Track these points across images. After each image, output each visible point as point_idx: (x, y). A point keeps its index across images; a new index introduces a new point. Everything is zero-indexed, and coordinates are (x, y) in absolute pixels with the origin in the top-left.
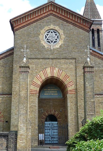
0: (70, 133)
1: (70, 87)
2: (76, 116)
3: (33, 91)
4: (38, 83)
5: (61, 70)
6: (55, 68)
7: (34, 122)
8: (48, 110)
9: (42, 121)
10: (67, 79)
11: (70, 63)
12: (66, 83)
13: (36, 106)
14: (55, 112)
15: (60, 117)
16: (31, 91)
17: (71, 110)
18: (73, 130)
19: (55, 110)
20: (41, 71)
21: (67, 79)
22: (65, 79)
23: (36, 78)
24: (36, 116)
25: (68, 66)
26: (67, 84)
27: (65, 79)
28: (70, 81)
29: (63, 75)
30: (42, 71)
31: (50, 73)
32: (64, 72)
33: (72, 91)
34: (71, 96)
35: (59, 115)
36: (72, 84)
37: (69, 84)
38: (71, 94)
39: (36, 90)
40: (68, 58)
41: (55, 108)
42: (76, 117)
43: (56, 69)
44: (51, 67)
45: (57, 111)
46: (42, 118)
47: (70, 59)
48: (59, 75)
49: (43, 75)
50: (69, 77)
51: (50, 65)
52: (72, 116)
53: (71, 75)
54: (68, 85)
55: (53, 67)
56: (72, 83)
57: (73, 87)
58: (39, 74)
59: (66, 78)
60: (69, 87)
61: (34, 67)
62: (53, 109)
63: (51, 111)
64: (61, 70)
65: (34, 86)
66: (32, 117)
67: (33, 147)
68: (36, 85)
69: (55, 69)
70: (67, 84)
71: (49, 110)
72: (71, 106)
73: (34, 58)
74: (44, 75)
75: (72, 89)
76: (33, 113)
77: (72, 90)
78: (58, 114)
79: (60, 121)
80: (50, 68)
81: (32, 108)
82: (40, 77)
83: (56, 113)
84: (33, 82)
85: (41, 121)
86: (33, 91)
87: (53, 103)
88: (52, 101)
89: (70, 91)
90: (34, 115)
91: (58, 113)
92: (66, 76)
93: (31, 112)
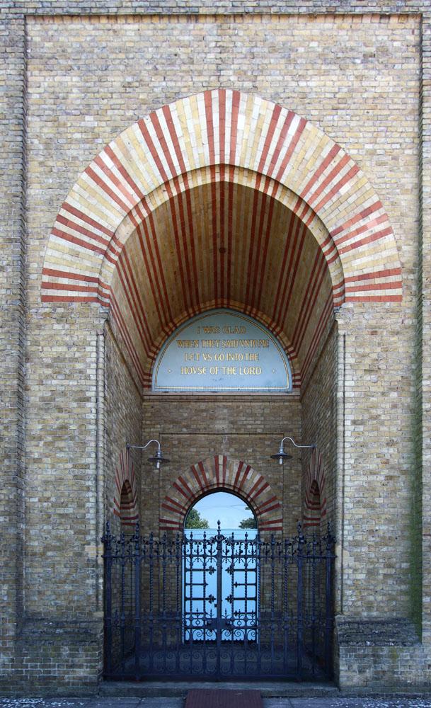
0: (348, 592)
1: (362, 254)
2: (404, 472)
3: (65, 281)
4: (103, 216)
5: (291, 115)
6: (243, 96)
7: (70, 510)
8: (201, 465)
9: (168, 525)
10: (344, 190)
11: (367, 58)
12: (332, 217)
13: (88, 399)
14: (242, 474)
15: (272, 504)
16: (46, 278)
17: (361, 428)
18: (370, 573)
19: (241, 464)
20: (130, 119)
21: (340, 185)
22: (327, 190)
23: (85, 176)
24: (87, 466)
25: (351, 81)
26: (340, 230)
27: (325, 184)
28: (367, 205)
29: (308, 156)
30: (136, 126)
31: (198, 137)
32: (321, 134)
33: (378, 281)
34: (368, 319)
35: (268, 488)
36: (381, 227)
37: (353, 228)
38: (367, 304)
39: (87, 274)
40: (358, 11)
41: (244, 450)
42: (403, 478)
43: (250, 102)
44: (215, 94)
45: (258, 470)
46: (165, 506)
47: (373, 15)
48: (277, 152)
49: (145, 160)
50: (355, 170)
51: (200, 73)
52: (372, 473)
53: (372, 153)
54: (346, 238)
55: (229, 93)
56: (379, 220)
57: (385, 254)
58: (113, 145)
59: (333, 175)
60: (351, 252)
61: (75, 94)
62: (232, 456)
63: (221, 468)
64: (291, 115)
65: (73, 240)
66: (60, 480)
67: (60, 690)
68: (86, 239)
69: (243, 106)
70: (340, 230)
71: (208, 464)
72: (367, 395)
73: (72, 16)
74: (149, 156)
75: (381, 268)
76: (61, 450)
77: (380, 274)
78: (259, 487)
79: (273, 525)
80: (201, 97)
81: (60, 410)
82: (122, 170)
83: (252, 478)
84: (64, 213)
85: (161, 521)
86: (65, 281)
87: (232, 423)
88: (225, 411)
89: (361, 283)
90: (71, 460)
91: (261, 479)
92: (337, 165)
93: (49, 439)
